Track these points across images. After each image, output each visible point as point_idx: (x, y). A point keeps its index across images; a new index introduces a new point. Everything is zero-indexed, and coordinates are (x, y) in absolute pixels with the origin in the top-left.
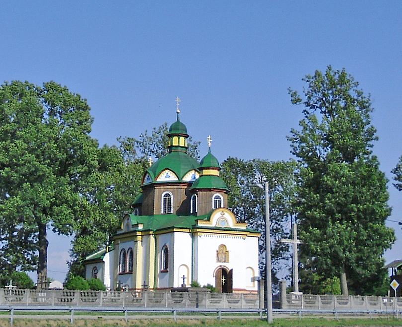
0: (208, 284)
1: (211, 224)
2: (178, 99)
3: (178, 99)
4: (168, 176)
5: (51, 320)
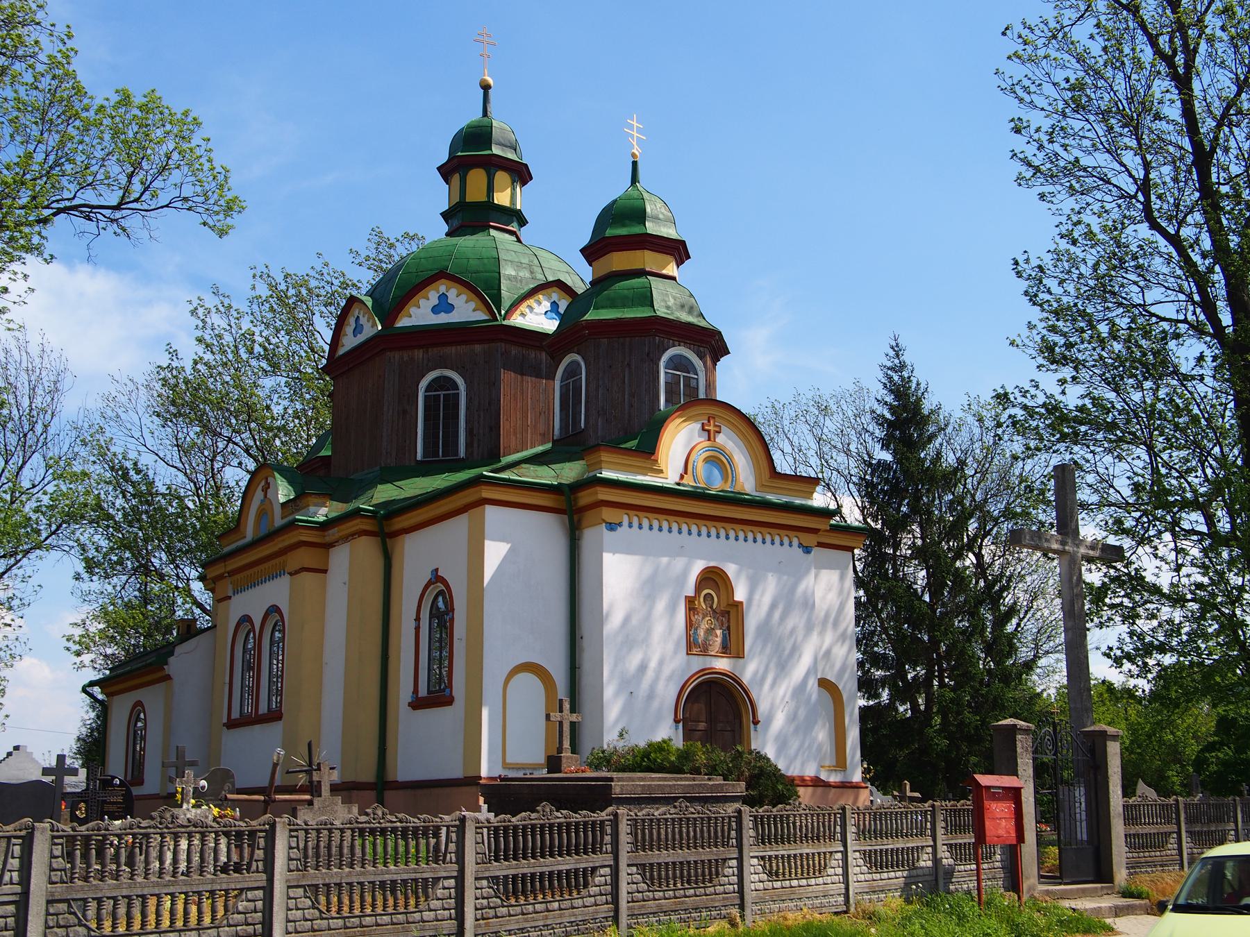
4: (444, 305)
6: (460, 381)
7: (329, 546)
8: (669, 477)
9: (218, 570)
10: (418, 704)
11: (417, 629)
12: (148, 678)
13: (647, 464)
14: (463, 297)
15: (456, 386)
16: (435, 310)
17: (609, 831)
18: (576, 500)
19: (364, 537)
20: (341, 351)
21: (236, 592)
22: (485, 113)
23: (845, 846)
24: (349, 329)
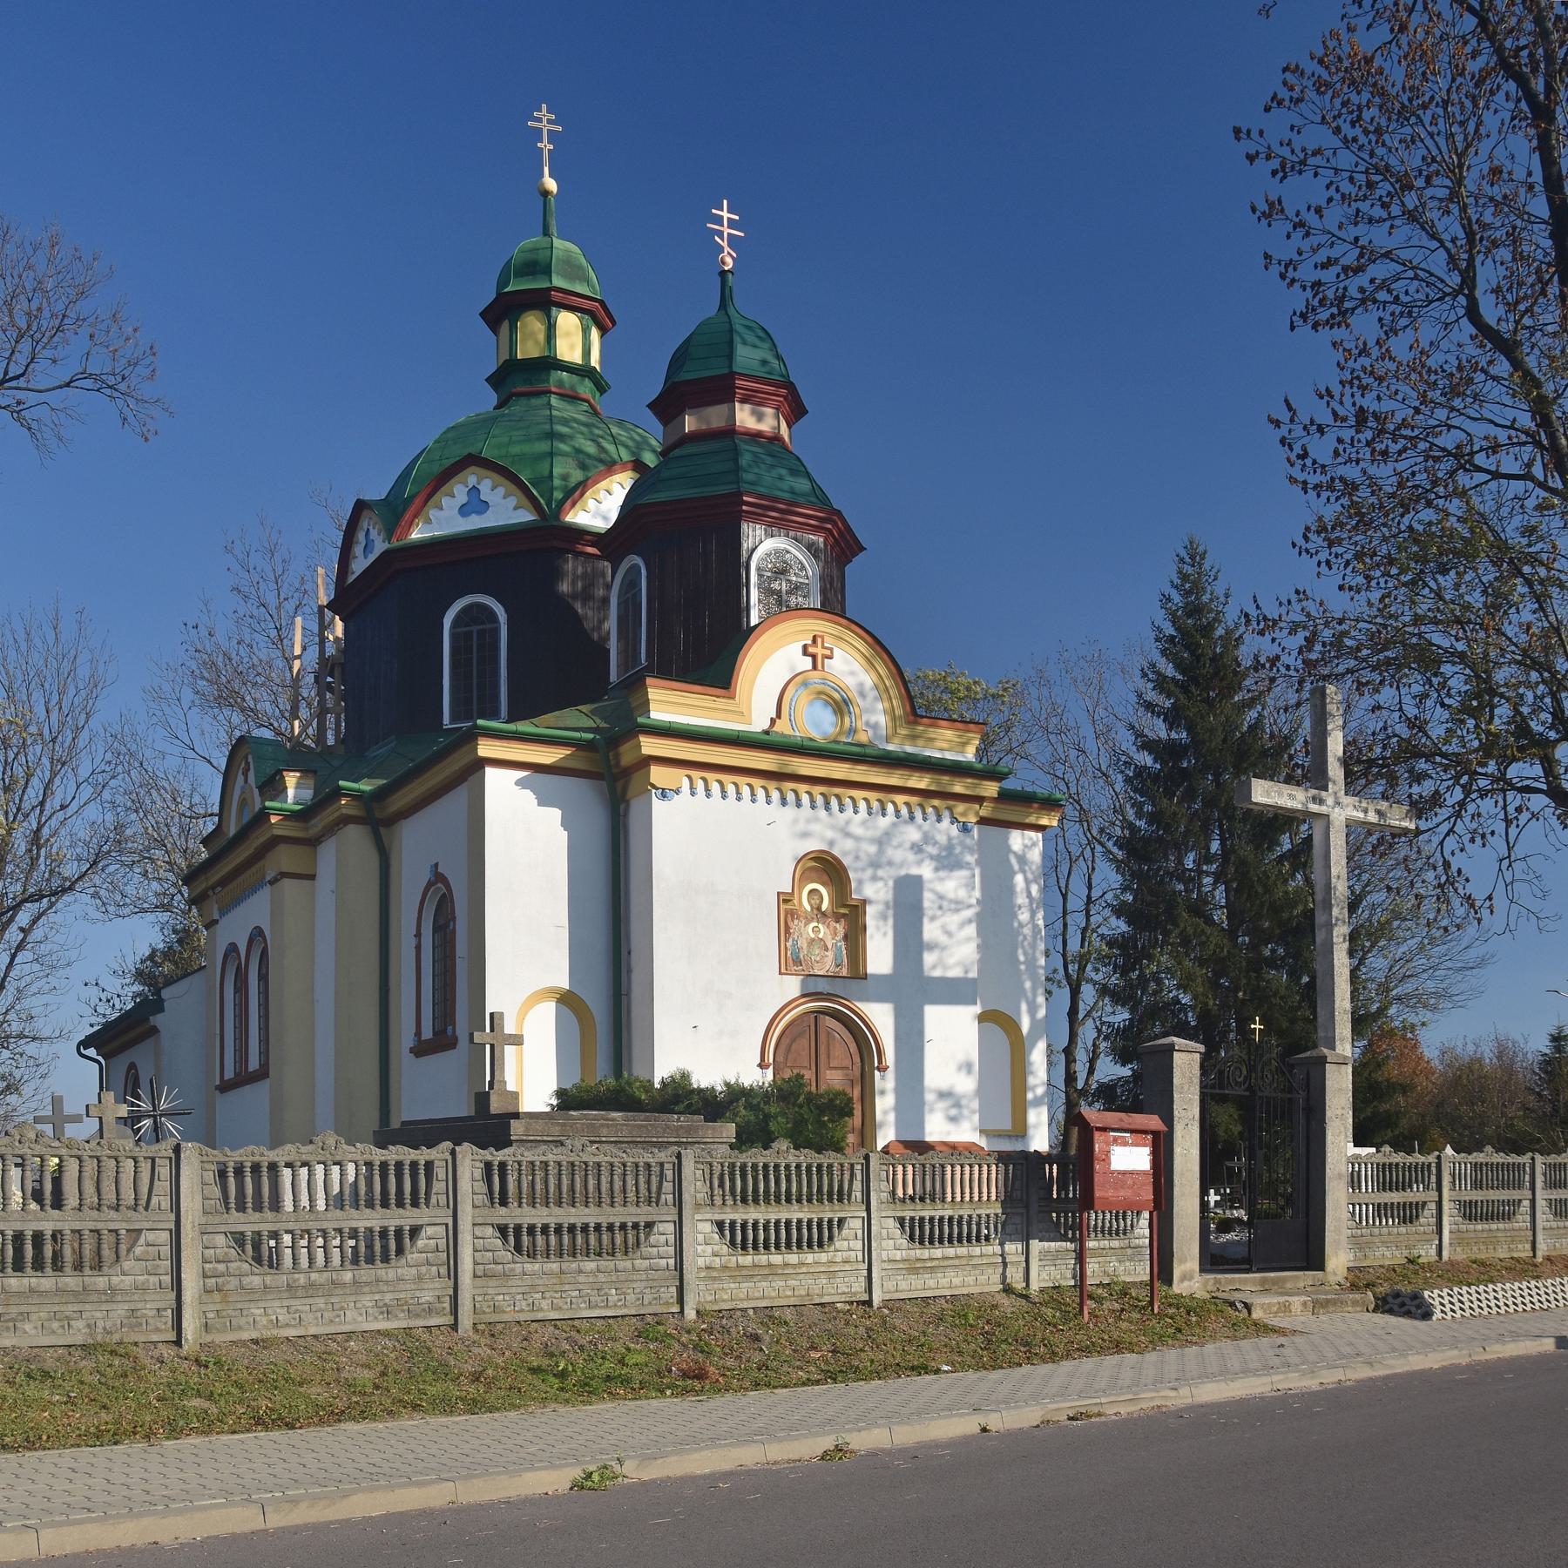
0: (727, 1084)
1: (741, 715)
2: (544, 113)
3: (544, 113)
4: (476, 504)
5: (1236, 1262)
6: (499, 609)
7: (313, 843)
8: (757, 722)
9: (201, 885)
10: (422, 1049)
11: (418, 948)
12: (132, 1034)
13: (721, 703)
14: (501, 491)
15: (493, 616)
16: (464, 511)
17: (442, 1175)
18: (617, 756)
19: (351, 826)
20: (351, 579)
21: (224, 911)
22: (723, 305)
23: (868, 1210)
24: (358, 550)
